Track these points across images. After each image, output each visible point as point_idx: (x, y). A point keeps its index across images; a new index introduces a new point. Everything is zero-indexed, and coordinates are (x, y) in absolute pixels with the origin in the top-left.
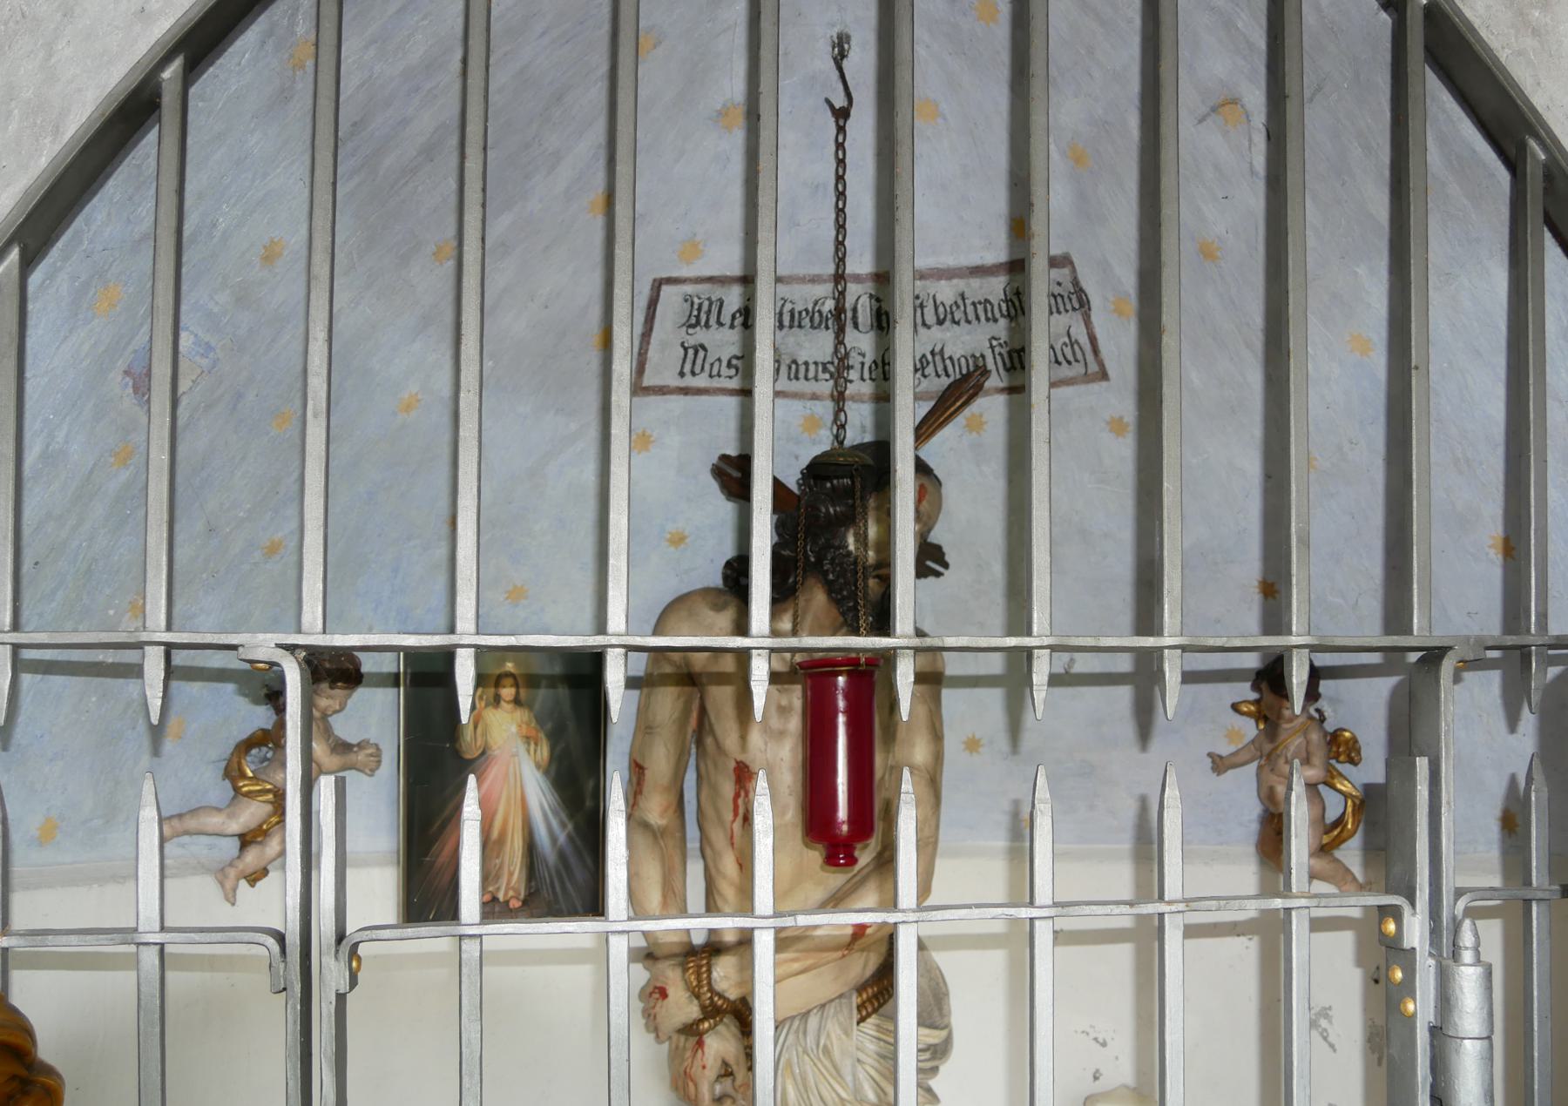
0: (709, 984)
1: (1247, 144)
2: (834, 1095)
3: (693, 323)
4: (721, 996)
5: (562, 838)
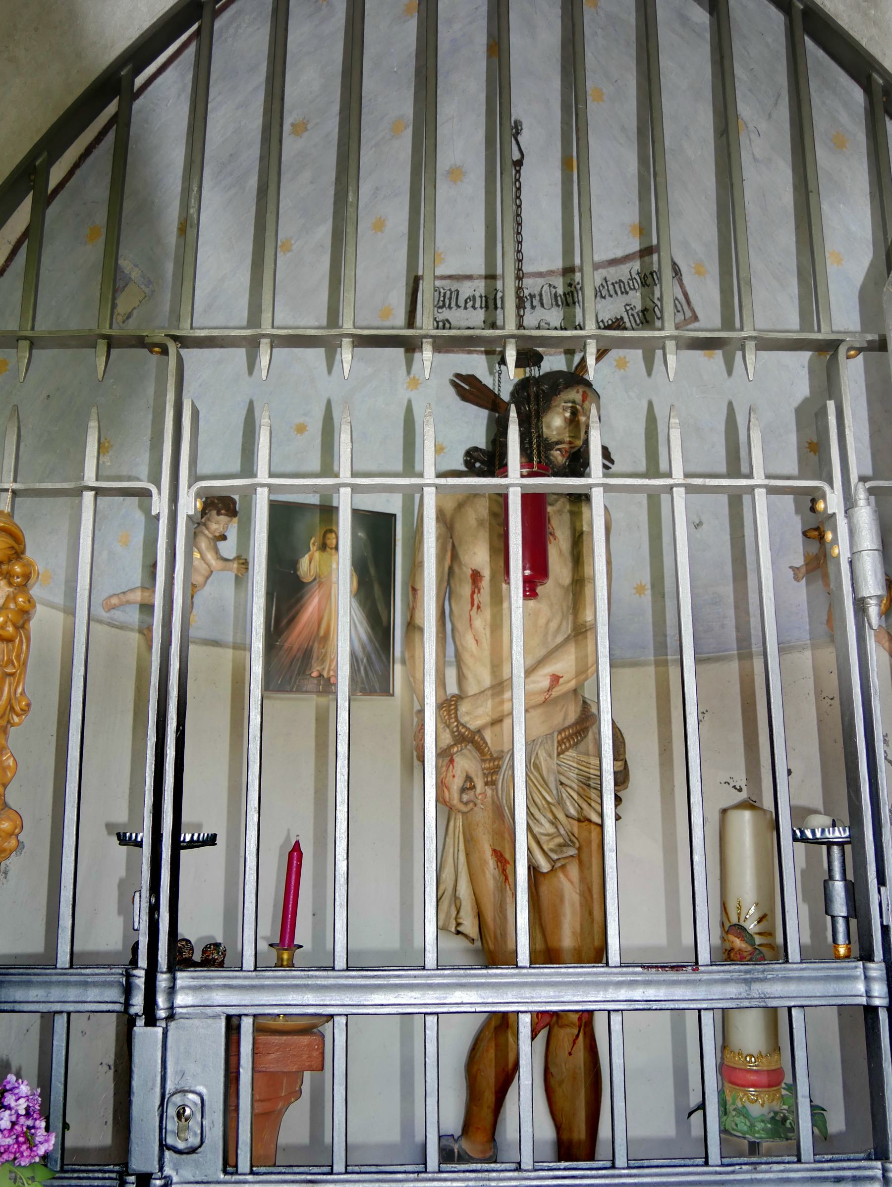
0: (456, 717)
1: (748, 142)
2: (544, 802)
3: (441, 305)
4: (464, 726)
5: (364, 637)
